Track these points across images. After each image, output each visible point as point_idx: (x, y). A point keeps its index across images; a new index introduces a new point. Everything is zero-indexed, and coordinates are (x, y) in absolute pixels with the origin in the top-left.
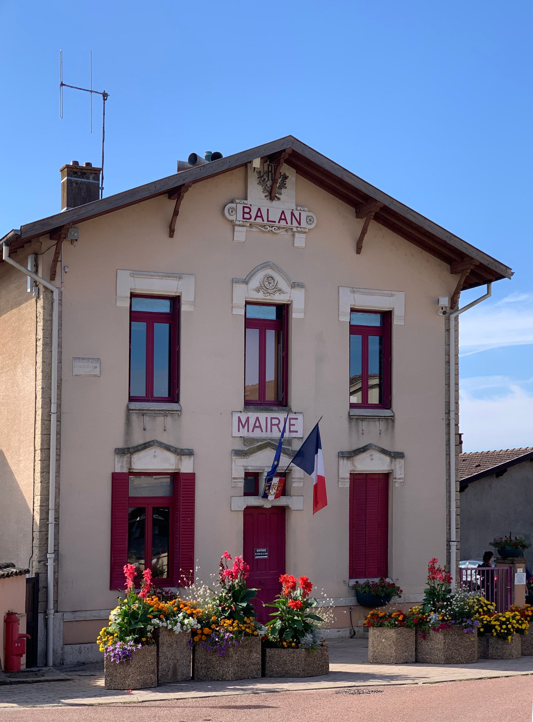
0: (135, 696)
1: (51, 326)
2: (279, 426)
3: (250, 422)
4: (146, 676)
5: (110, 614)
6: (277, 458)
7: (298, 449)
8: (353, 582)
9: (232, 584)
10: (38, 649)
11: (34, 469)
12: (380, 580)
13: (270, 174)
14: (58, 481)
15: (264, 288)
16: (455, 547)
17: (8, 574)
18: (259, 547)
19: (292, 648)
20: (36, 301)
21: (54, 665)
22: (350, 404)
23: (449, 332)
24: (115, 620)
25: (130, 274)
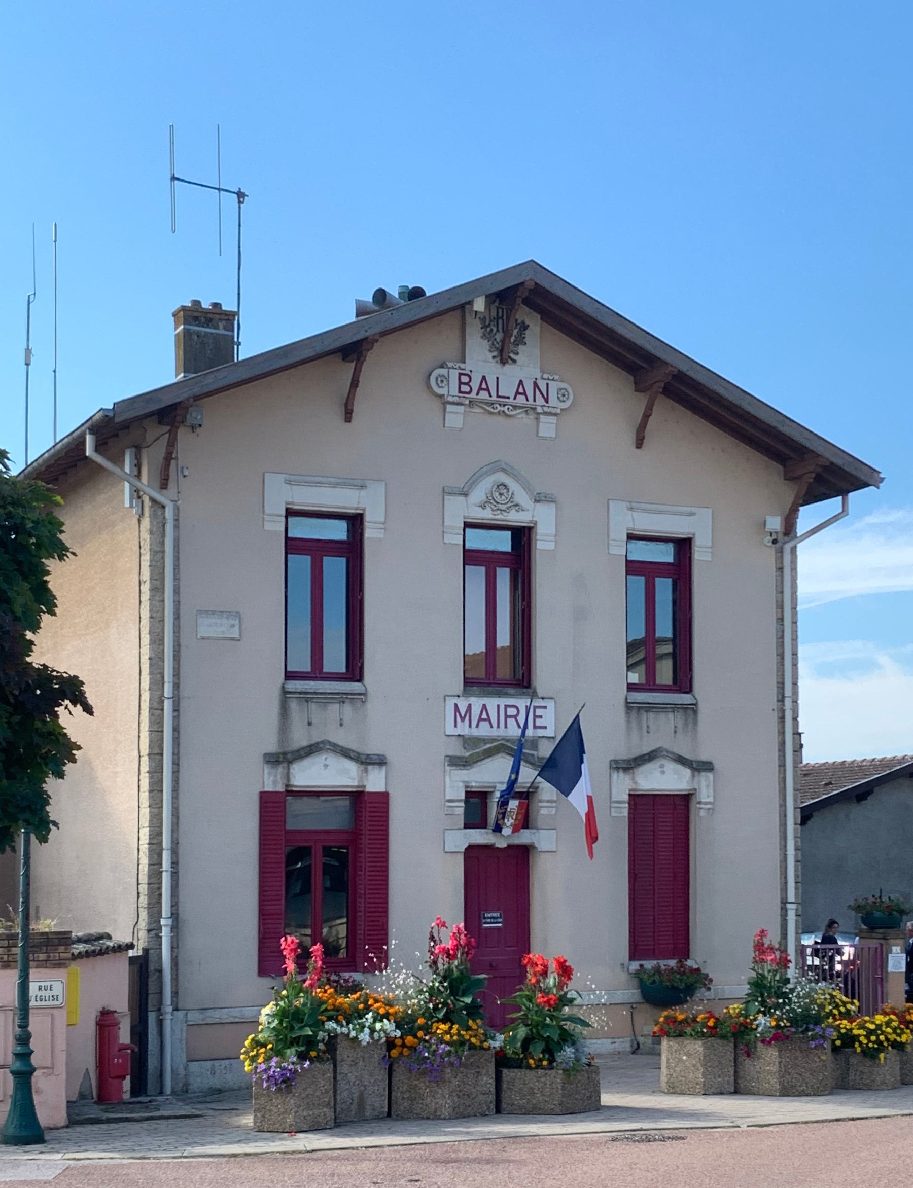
4: (316, 1112)
6: (516, 770)
7: (548, 756)
8: (635, 966)
9: (449, 968)
11: (139, 787)
12: (678, 962)
14: (175, 805)
15: (492, 501)
17: (101, 950)
20: (139, 521)
21: (174, 1093)
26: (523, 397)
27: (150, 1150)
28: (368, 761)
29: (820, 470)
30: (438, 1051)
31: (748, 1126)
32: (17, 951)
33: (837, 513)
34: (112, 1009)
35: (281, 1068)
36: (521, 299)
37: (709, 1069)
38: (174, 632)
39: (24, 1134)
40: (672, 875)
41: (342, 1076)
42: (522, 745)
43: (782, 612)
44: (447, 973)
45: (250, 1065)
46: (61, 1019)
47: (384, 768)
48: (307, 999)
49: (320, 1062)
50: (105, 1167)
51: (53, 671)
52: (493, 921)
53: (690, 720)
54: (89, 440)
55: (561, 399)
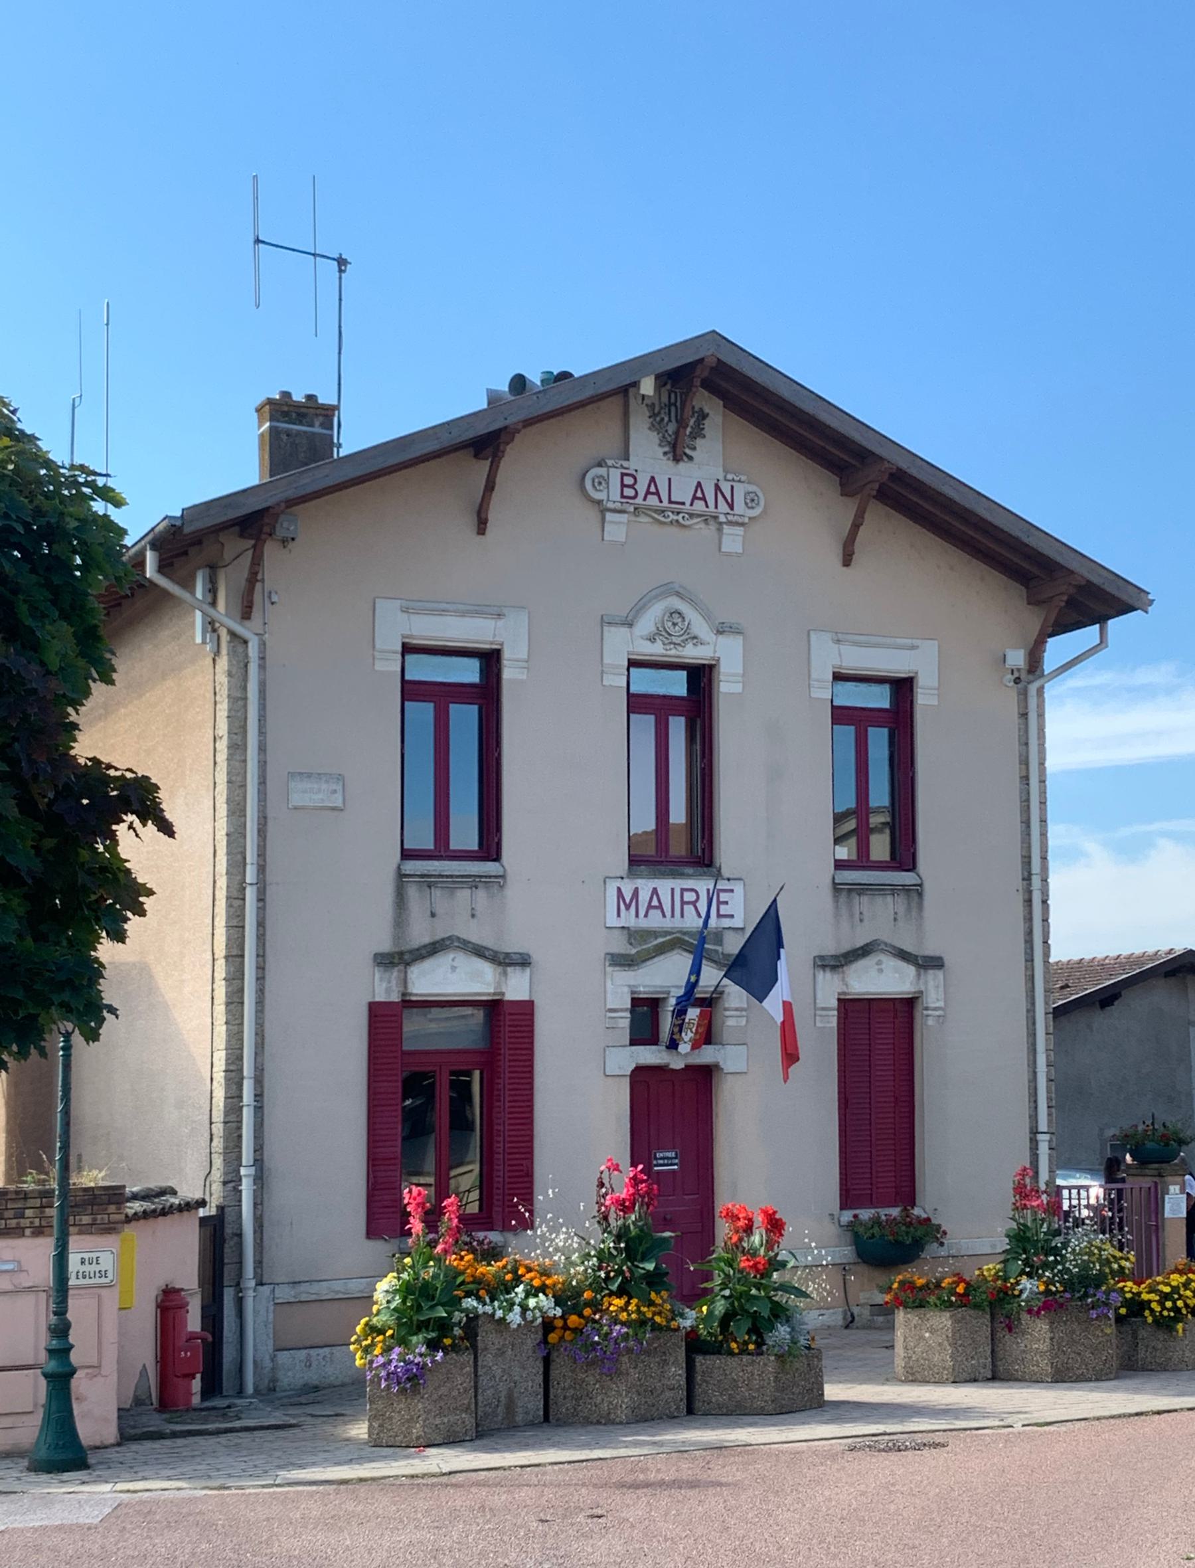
0: (435, 1462)
1: (243, 710)
2: (698, 905)
3: (640, 898)
4: (452, 1418)
5: (376, 1290)
6: (696, 970)
7: (736, 951)
8: (847, 1216)
9: (624, 1224)
10: (225, 1360)
11: (213, 998)
12: (902, 1211)
13: (673, 409)
14: (260, 1021)
15: (664, 633)
16: (1047, 1143)
17: (163, 1209)
18: (659, 1149)
19: (749, 1354)
20: (214, 660)
21: (257, 1392)
22: (836, 861)
23: (1027, 719)
24: (388, 1302)
25: (401, 607)
26: (702, 503)
27: (230, 1476)
28: (507, 961)
29: (1072, 591)
30: (612, 1333)
31: (1023, 1426)
32: (53, 1212)
33: (1095, 644)
34: (178, 1286)
35: (404, 1361)
36: (699, 380)
37: (960, 1349)
38: (259, 801)
39: (62, 1457)
40: (892, 1099)
41: (484, 1370)
42: (704, 937)
43: (1027, 769)
44: (623, 1231)
45: (362, 1358)
46: (111, 1301)
47: (528, 970)
48: (439, 1268)
49: (457, 1353)
50: (172, 1502)
51: (109, 767)
52: (667, 1161)
53: (914, 905)
54: (150, 558)
55: (750, 505)
